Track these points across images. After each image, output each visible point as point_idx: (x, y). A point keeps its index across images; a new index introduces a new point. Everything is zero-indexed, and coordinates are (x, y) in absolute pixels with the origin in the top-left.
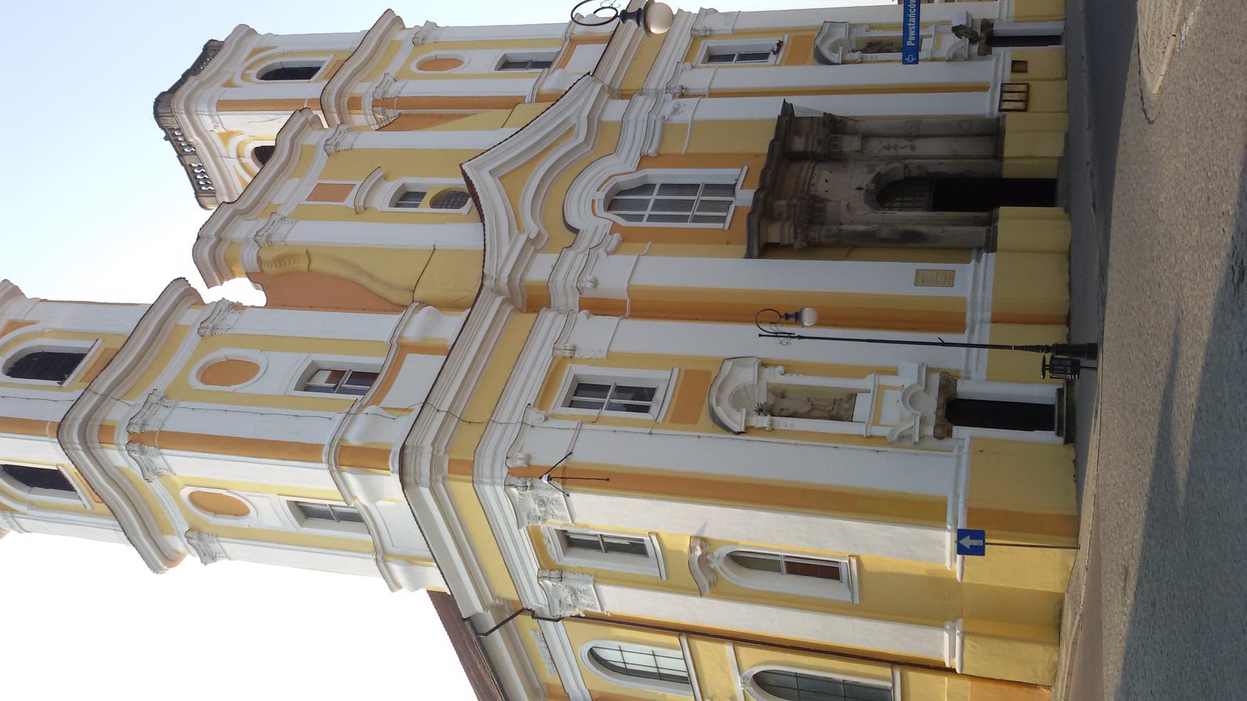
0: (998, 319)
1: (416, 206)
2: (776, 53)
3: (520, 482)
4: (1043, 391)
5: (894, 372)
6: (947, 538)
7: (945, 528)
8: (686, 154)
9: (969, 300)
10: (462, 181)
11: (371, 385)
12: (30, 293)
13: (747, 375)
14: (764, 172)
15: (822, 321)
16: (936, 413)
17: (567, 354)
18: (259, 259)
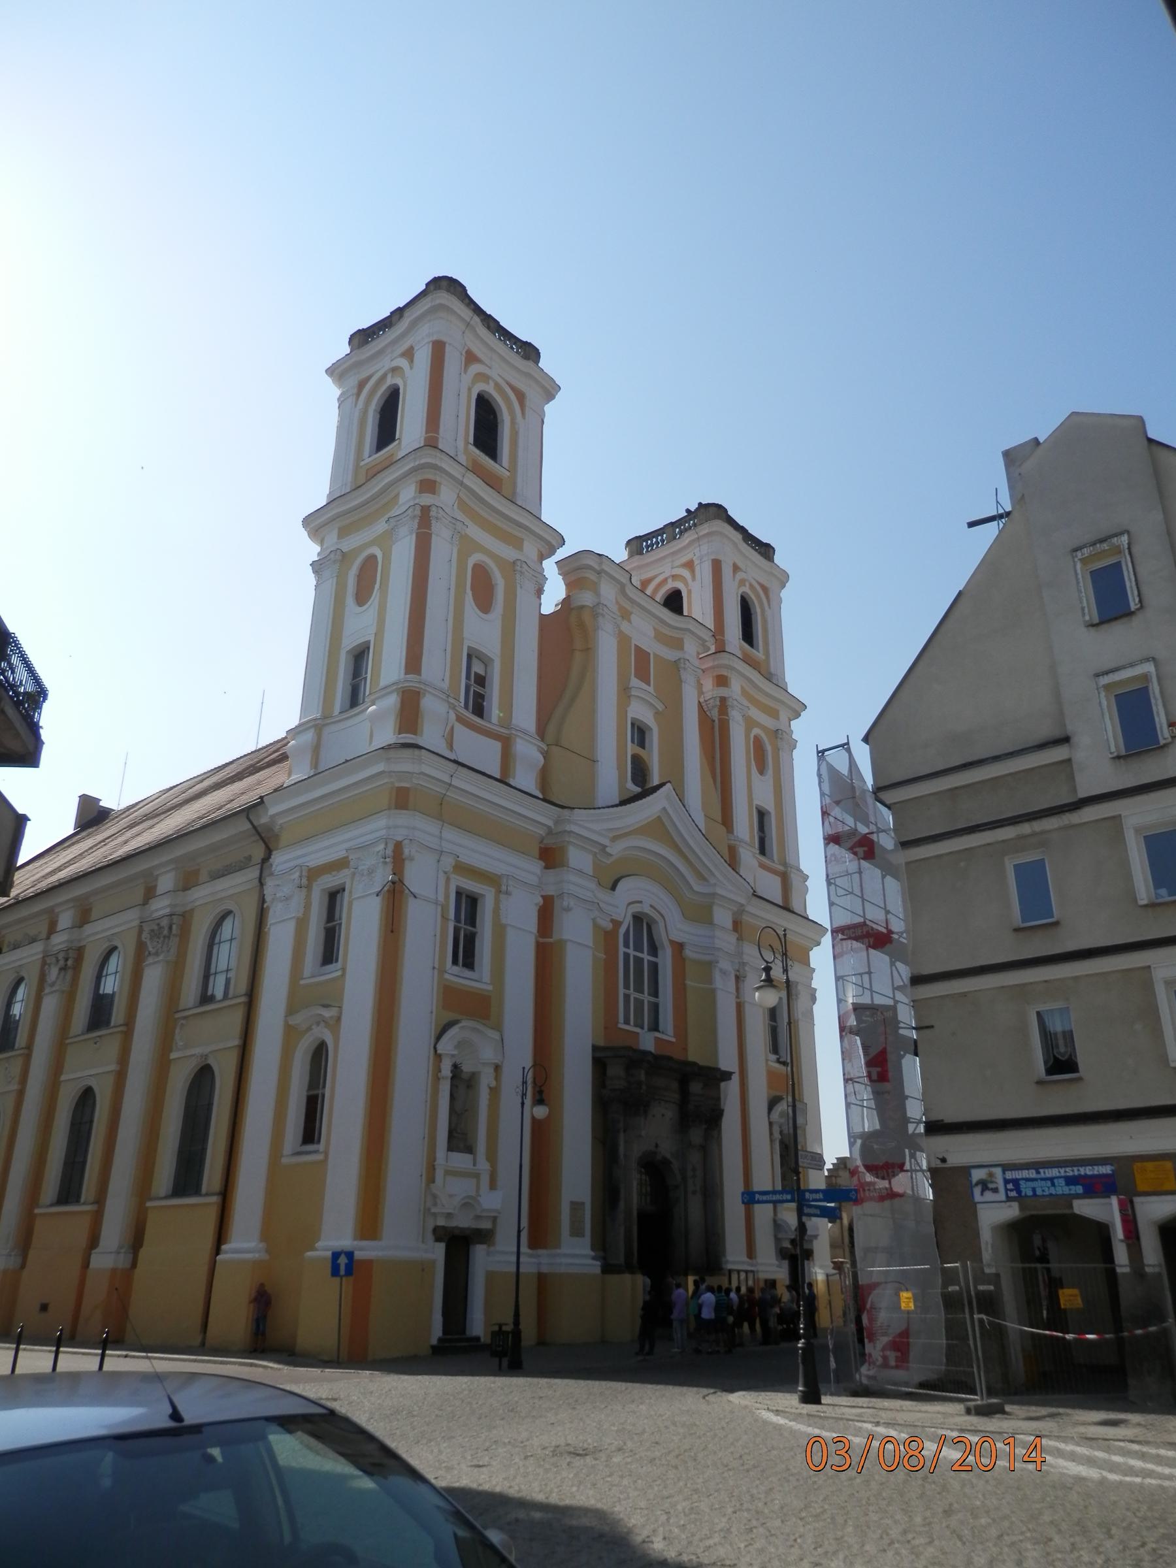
0: (542, 1278)
1: (633, 742)
2: (778, 1061)
3: (389, 852)
4: (478, 1325)
5: (493, 1185)
6: (345, 1242)
7: (355, 1239)
8: (685, 985)
9: (558, 1251)
10: (656, 782)
11: (473, 713)
12: (548, 408)
13: (488, 1054)
14: (669, 1058)
15: (537, 1125)
16: (456, 1227)
17: (504, 888)
18: (582, 607)
